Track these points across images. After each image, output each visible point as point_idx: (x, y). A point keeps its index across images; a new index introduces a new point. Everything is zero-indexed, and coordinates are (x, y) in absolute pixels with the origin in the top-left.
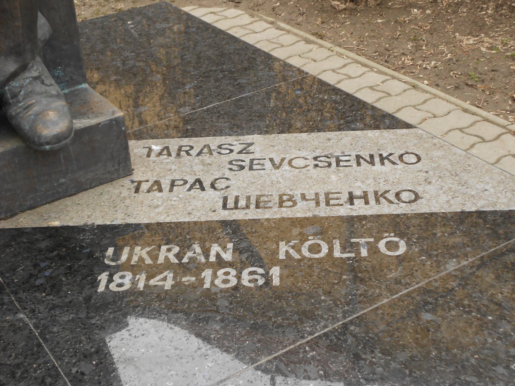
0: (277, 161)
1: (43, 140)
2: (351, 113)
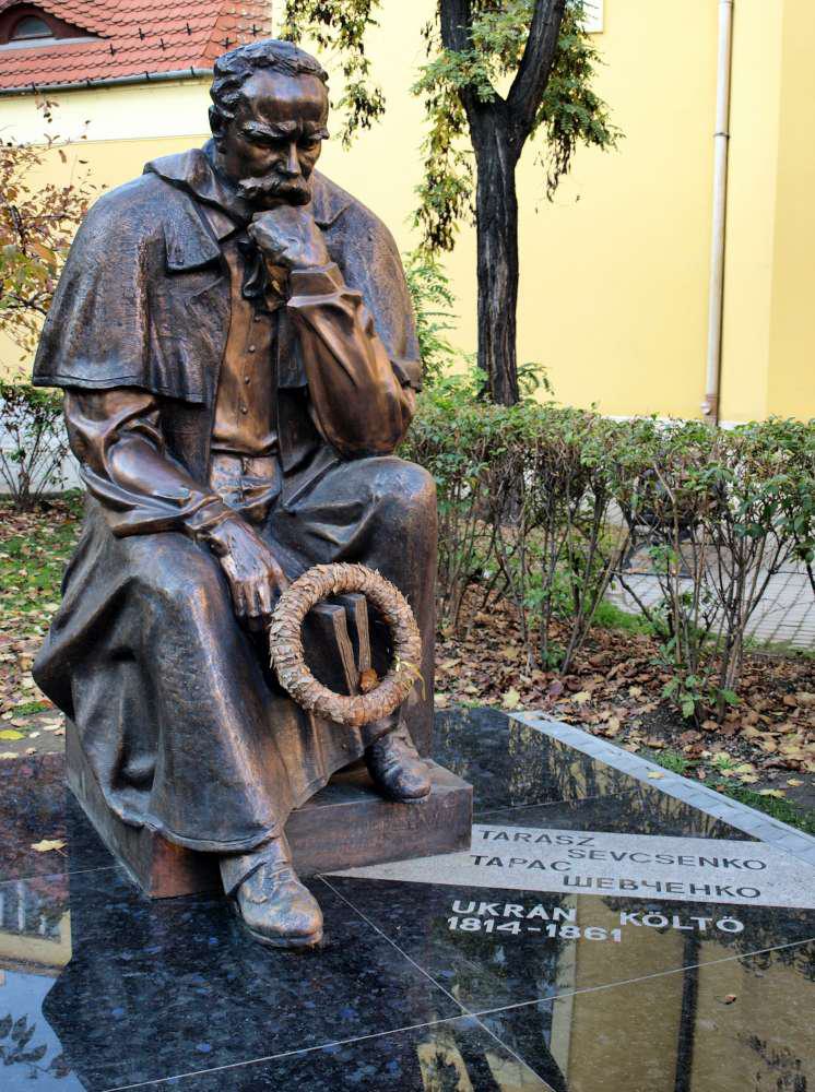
0: (618, 854)
1: (407, 792)
2: (685, 821)
